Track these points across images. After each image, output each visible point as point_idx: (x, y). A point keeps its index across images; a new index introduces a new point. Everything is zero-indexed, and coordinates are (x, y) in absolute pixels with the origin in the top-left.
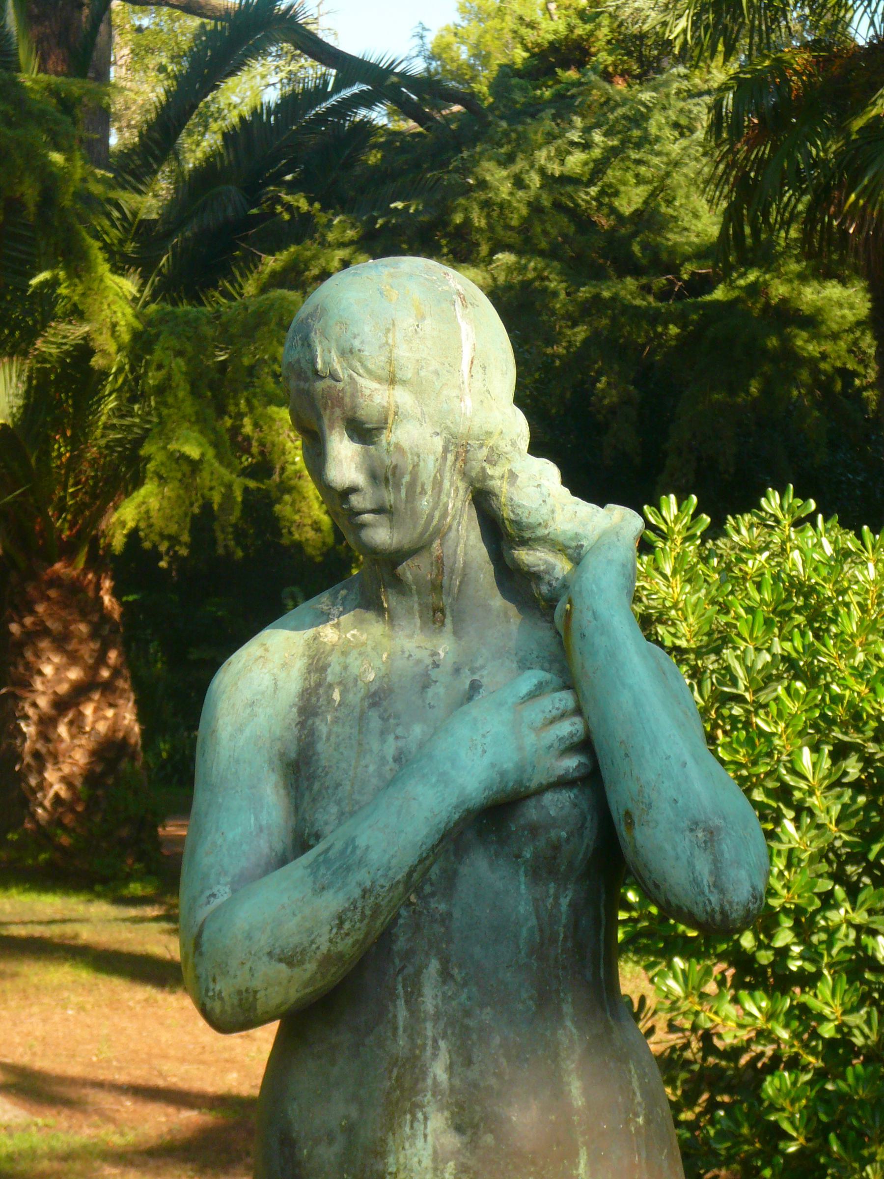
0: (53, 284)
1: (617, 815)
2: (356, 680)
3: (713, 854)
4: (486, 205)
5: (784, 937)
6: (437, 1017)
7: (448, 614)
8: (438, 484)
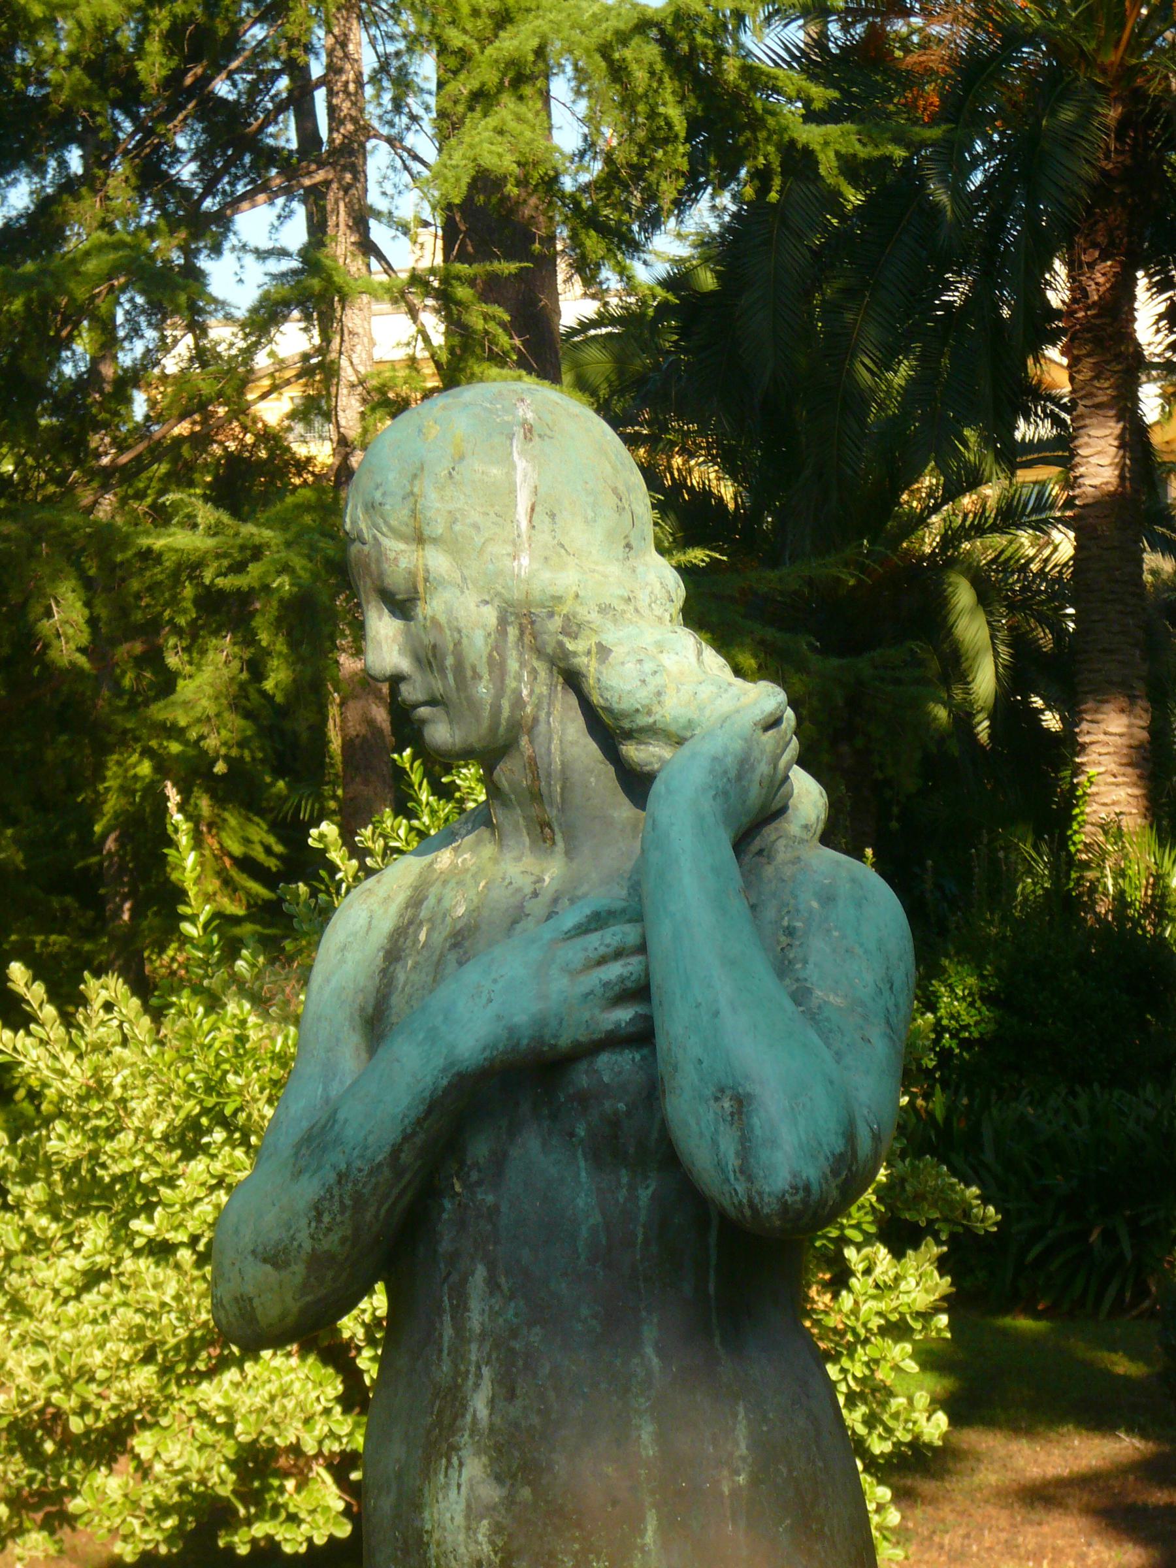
2: (445, 916)
3: (742, 1130)
6: (483, 1336)
7: (556, 829)
8: (498, 667)
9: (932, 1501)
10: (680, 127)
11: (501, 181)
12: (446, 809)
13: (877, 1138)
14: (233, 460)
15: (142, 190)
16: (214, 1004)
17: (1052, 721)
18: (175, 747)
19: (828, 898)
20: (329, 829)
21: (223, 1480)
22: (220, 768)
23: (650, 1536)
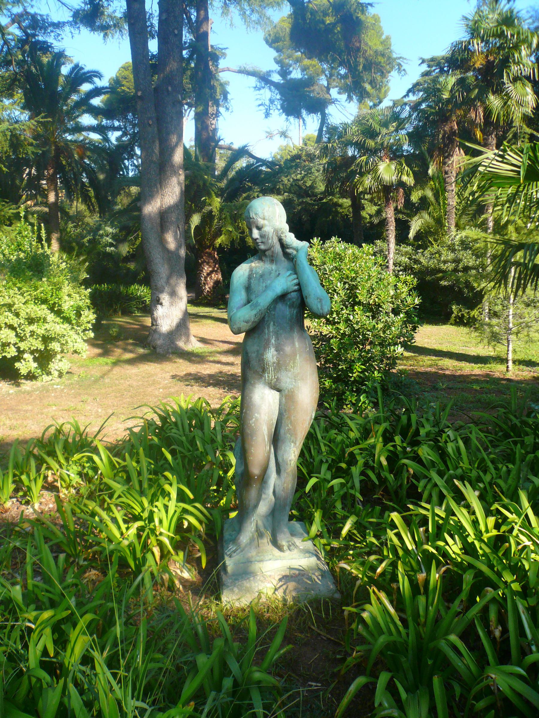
0: (206, 199)
1: (304, 297)
4: (283, 184)
5: (334, 316)
8: (272, 238)
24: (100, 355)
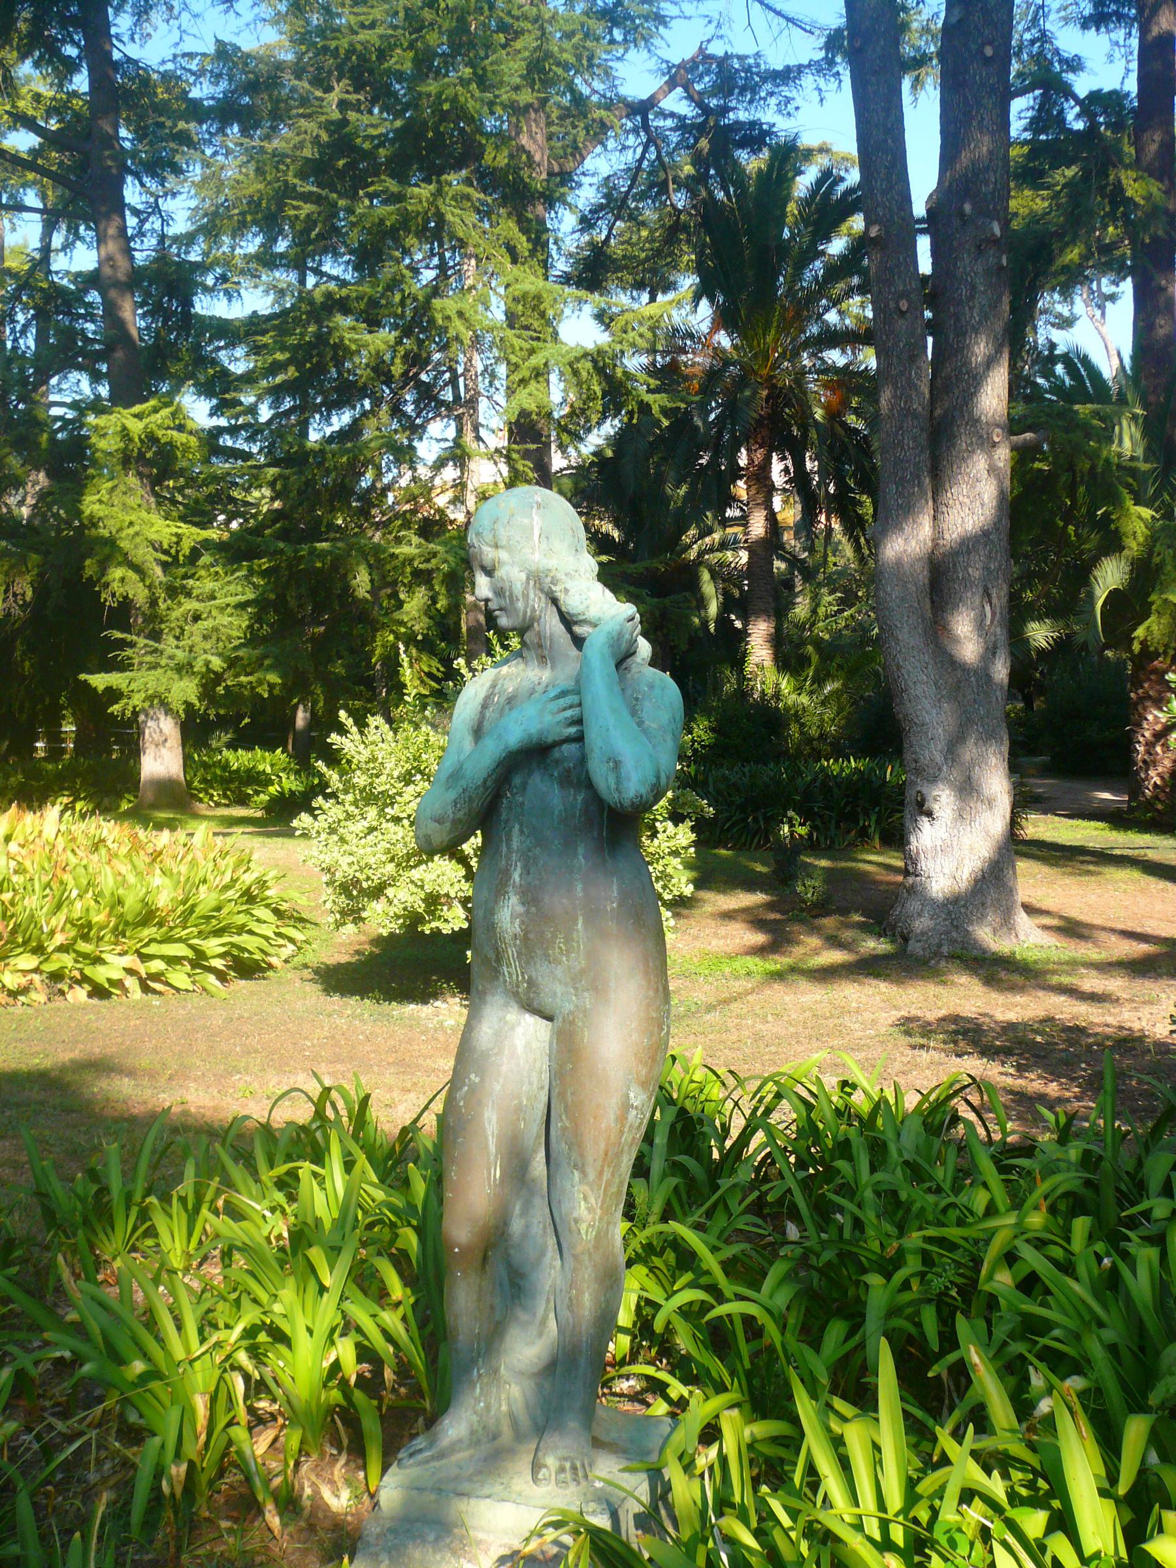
8: (526, 596)
9: (687, 917)
10: (599, 394)
11: (530, 414)
12: (505, 654)
13: (668, 778)
14: (425, 519)
15: (392, 416)
16: (417, 727)
17: (738, 624)
18: (403, 630)
19: (651, 687)
20: (461, 661)
21: (421, 908)
22: (420, 637)
23: (580, 926)
24: (760, 951)
